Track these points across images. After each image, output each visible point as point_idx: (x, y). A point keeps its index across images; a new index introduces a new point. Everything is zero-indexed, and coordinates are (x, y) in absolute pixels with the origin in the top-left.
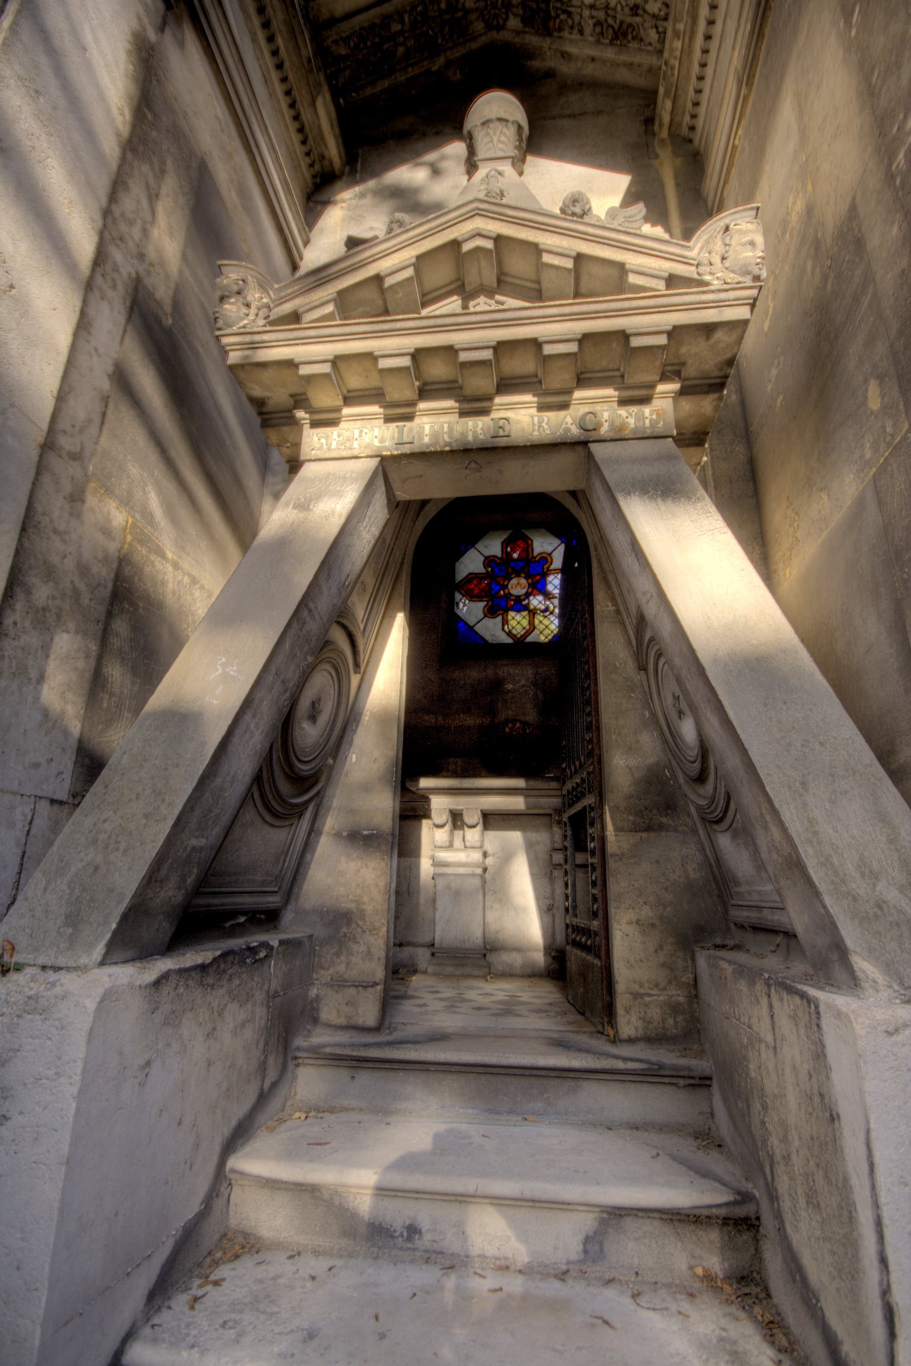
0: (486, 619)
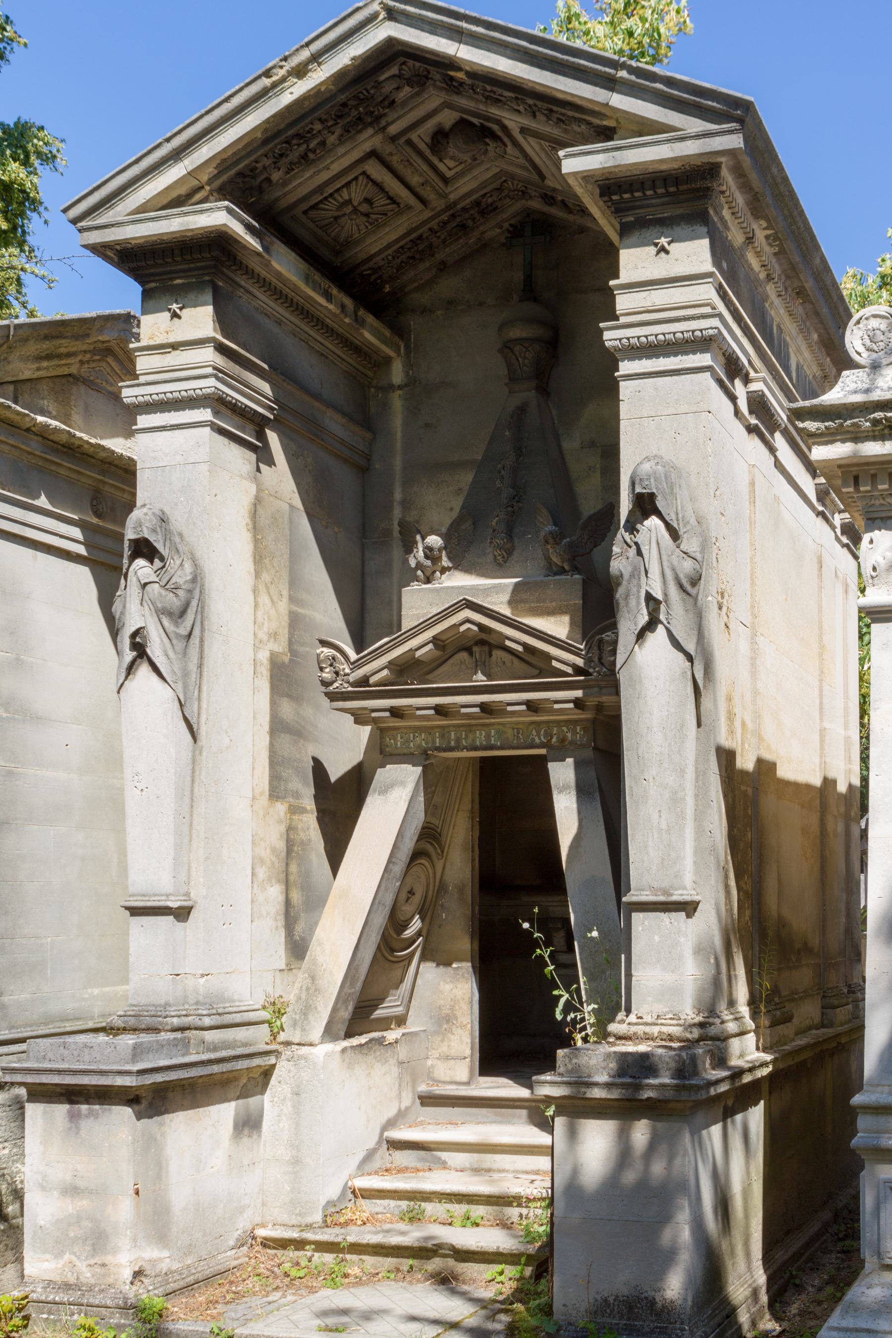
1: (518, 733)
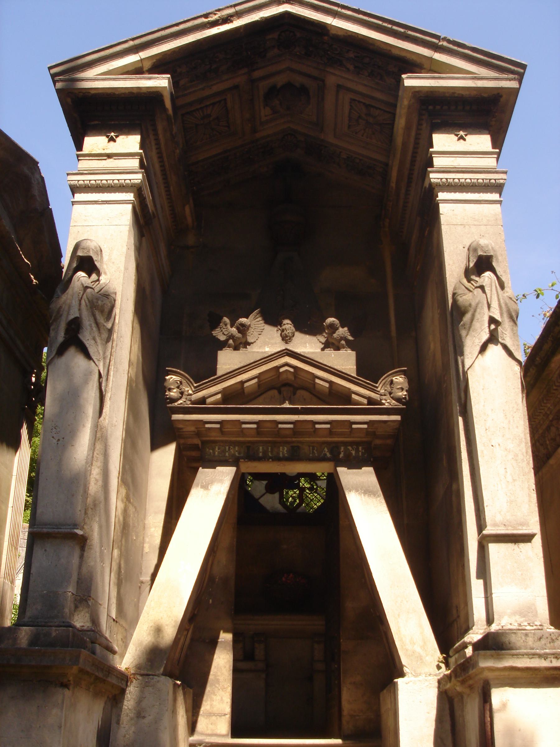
0: (268, 494)
1: (313, 449)
